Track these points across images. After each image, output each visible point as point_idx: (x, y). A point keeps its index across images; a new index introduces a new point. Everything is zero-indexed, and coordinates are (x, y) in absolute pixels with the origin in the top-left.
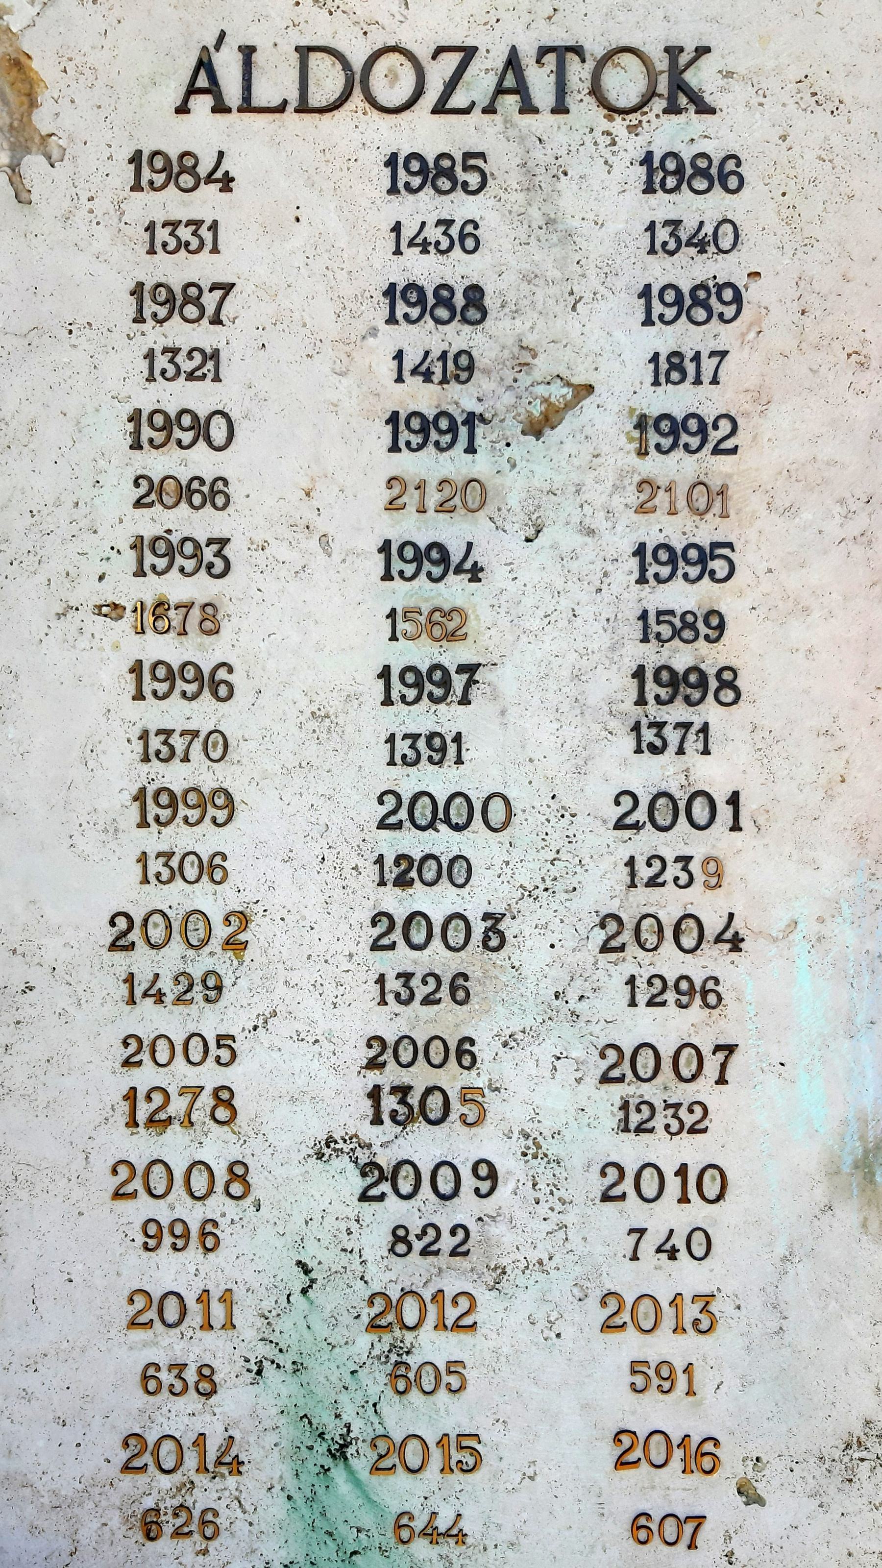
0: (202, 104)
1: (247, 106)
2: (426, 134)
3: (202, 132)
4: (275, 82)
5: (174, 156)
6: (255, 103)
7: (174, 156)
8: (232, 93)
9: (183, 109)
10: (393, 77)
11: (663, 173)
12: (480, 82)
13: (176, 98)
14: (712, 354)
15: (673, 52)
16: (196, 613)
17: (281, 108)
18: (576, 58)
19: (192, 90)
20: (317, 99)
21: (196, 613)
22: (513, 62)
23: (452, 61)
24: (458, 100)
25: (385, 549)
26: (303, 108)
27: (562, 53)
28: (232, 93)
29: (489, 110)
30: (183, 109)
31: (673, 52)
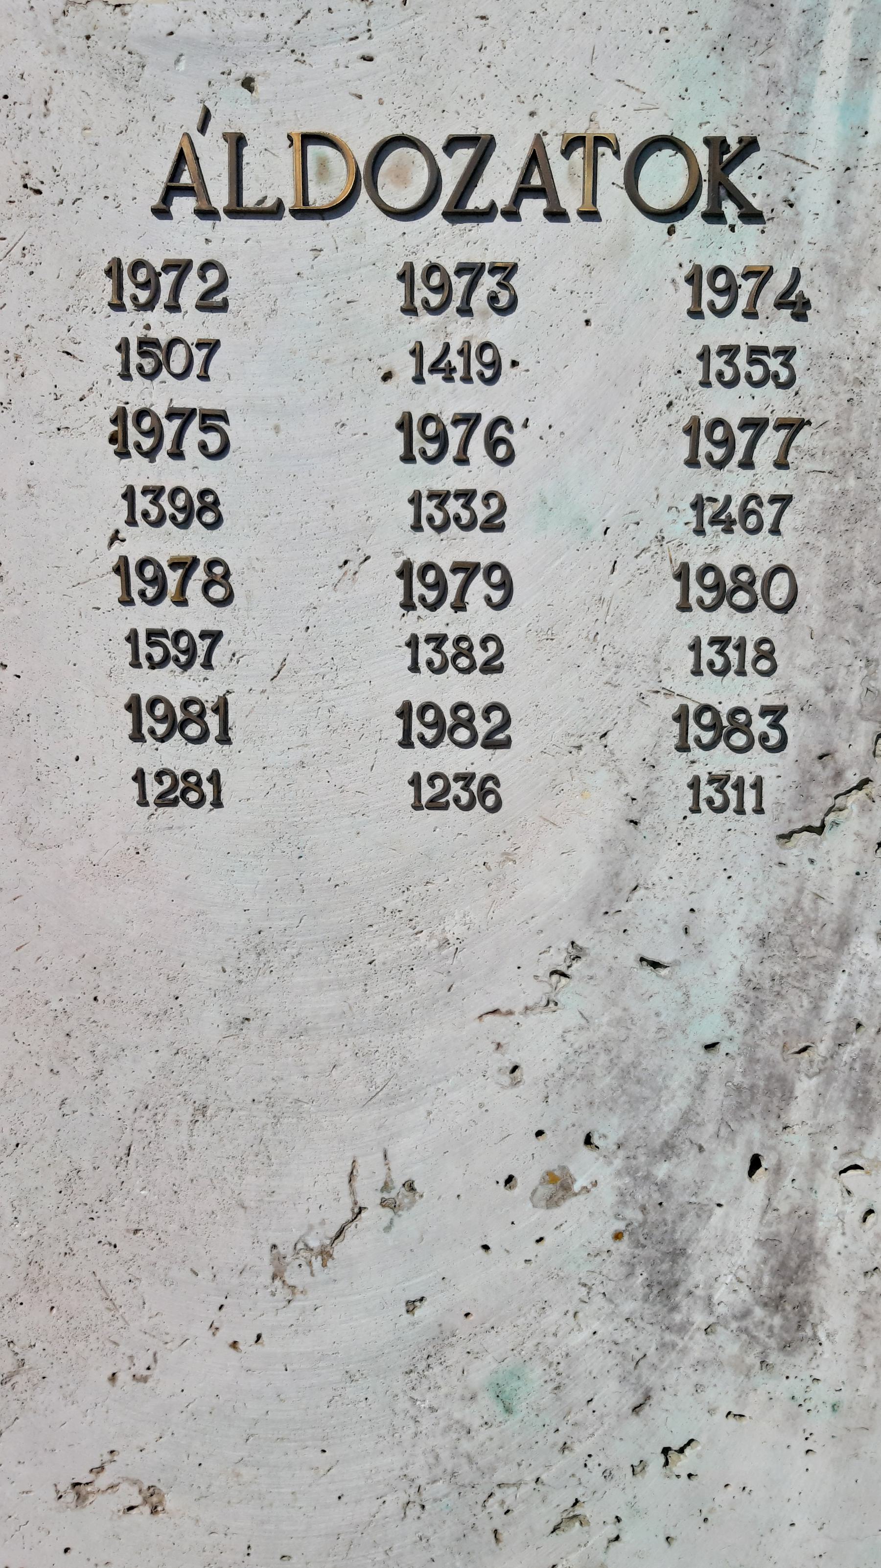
0: (183, 205)
1: (237, 211)
2: (441, 242)
3: (185, 235)
4: (270, 175)
5: (724, 711)
6: (249, 200)
7: (724, 711)
8: (220, 197)
9: (162, 212)
10: (402, 178)
11: (713, 289)
12: (497, 185)
13: (155, 199)
14: (774, 499)
15: (716, 145)
16: (200, 575)
17: (275, 212)
18: (609, 152)
19: (172, 189)
20: (319, 197)
21: (200, 575)
22: (536, 159)
23: (465, 155)
24: (477, 201)
25: (405, 712)
26: (304, 212)
27: (589, 145)
28: (220, 197)
29: (512, 214)
30: (162, 212)
31: (716, 145)
